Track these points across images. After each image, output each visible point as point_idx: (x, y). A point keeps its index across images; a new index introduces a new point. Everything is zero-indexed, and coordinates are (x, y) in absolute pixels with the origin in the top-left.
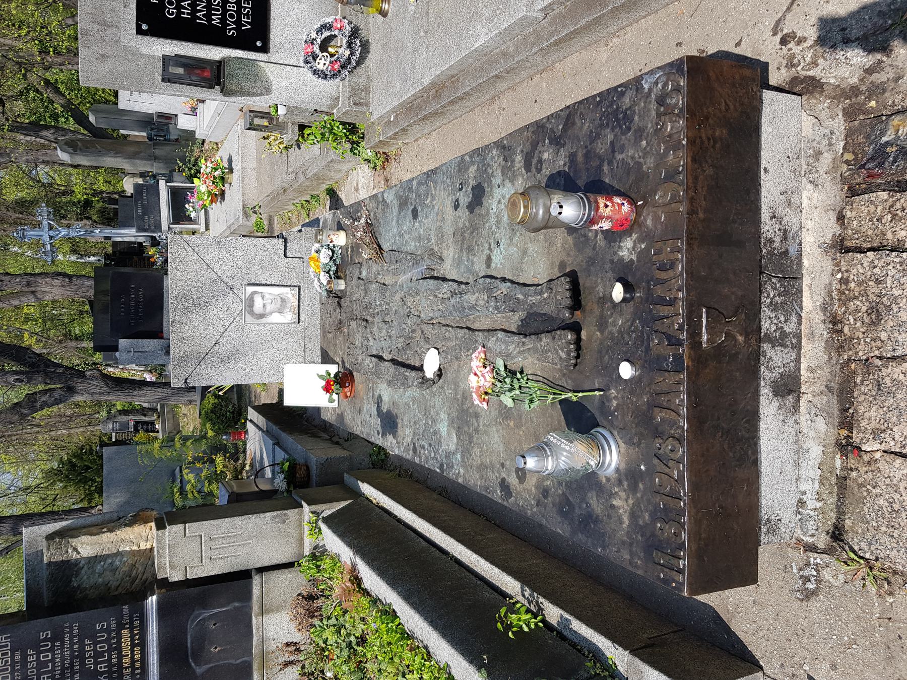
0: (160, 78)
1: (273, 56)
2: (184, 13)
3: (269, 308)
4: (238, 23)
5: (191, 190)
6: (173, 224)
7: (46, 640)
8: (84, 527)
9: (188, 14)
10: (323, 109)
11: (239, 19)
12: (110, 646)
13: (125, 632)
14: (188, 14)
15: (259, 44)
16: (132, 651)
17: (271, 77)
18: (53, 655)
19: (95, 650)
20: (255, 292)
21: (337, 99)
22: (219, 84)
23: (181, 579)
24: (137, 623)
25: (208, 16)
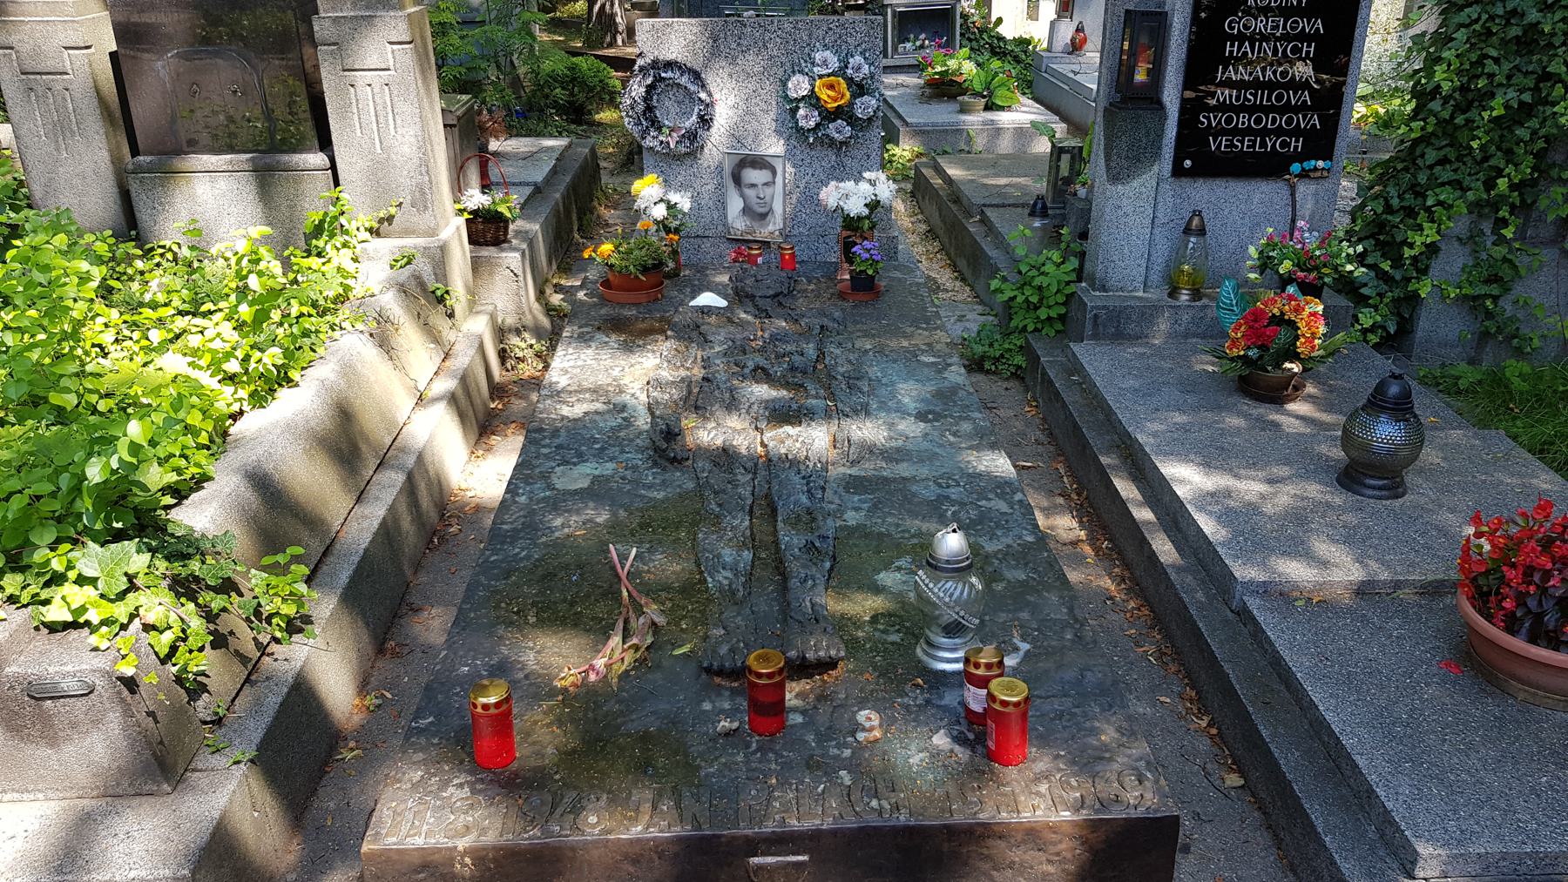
2: (1232, 46)
3: (750, 192)
6: (894, 13)
9: (1231, 52)
10: (1088, 265)
11: (1224, 132)
14: (1231, 52)
17: (1135, 184)
20: (774, 173)
21: (1104, 288)
22: (1123, 100)
23: (316, 36)
25: (1228, 83)
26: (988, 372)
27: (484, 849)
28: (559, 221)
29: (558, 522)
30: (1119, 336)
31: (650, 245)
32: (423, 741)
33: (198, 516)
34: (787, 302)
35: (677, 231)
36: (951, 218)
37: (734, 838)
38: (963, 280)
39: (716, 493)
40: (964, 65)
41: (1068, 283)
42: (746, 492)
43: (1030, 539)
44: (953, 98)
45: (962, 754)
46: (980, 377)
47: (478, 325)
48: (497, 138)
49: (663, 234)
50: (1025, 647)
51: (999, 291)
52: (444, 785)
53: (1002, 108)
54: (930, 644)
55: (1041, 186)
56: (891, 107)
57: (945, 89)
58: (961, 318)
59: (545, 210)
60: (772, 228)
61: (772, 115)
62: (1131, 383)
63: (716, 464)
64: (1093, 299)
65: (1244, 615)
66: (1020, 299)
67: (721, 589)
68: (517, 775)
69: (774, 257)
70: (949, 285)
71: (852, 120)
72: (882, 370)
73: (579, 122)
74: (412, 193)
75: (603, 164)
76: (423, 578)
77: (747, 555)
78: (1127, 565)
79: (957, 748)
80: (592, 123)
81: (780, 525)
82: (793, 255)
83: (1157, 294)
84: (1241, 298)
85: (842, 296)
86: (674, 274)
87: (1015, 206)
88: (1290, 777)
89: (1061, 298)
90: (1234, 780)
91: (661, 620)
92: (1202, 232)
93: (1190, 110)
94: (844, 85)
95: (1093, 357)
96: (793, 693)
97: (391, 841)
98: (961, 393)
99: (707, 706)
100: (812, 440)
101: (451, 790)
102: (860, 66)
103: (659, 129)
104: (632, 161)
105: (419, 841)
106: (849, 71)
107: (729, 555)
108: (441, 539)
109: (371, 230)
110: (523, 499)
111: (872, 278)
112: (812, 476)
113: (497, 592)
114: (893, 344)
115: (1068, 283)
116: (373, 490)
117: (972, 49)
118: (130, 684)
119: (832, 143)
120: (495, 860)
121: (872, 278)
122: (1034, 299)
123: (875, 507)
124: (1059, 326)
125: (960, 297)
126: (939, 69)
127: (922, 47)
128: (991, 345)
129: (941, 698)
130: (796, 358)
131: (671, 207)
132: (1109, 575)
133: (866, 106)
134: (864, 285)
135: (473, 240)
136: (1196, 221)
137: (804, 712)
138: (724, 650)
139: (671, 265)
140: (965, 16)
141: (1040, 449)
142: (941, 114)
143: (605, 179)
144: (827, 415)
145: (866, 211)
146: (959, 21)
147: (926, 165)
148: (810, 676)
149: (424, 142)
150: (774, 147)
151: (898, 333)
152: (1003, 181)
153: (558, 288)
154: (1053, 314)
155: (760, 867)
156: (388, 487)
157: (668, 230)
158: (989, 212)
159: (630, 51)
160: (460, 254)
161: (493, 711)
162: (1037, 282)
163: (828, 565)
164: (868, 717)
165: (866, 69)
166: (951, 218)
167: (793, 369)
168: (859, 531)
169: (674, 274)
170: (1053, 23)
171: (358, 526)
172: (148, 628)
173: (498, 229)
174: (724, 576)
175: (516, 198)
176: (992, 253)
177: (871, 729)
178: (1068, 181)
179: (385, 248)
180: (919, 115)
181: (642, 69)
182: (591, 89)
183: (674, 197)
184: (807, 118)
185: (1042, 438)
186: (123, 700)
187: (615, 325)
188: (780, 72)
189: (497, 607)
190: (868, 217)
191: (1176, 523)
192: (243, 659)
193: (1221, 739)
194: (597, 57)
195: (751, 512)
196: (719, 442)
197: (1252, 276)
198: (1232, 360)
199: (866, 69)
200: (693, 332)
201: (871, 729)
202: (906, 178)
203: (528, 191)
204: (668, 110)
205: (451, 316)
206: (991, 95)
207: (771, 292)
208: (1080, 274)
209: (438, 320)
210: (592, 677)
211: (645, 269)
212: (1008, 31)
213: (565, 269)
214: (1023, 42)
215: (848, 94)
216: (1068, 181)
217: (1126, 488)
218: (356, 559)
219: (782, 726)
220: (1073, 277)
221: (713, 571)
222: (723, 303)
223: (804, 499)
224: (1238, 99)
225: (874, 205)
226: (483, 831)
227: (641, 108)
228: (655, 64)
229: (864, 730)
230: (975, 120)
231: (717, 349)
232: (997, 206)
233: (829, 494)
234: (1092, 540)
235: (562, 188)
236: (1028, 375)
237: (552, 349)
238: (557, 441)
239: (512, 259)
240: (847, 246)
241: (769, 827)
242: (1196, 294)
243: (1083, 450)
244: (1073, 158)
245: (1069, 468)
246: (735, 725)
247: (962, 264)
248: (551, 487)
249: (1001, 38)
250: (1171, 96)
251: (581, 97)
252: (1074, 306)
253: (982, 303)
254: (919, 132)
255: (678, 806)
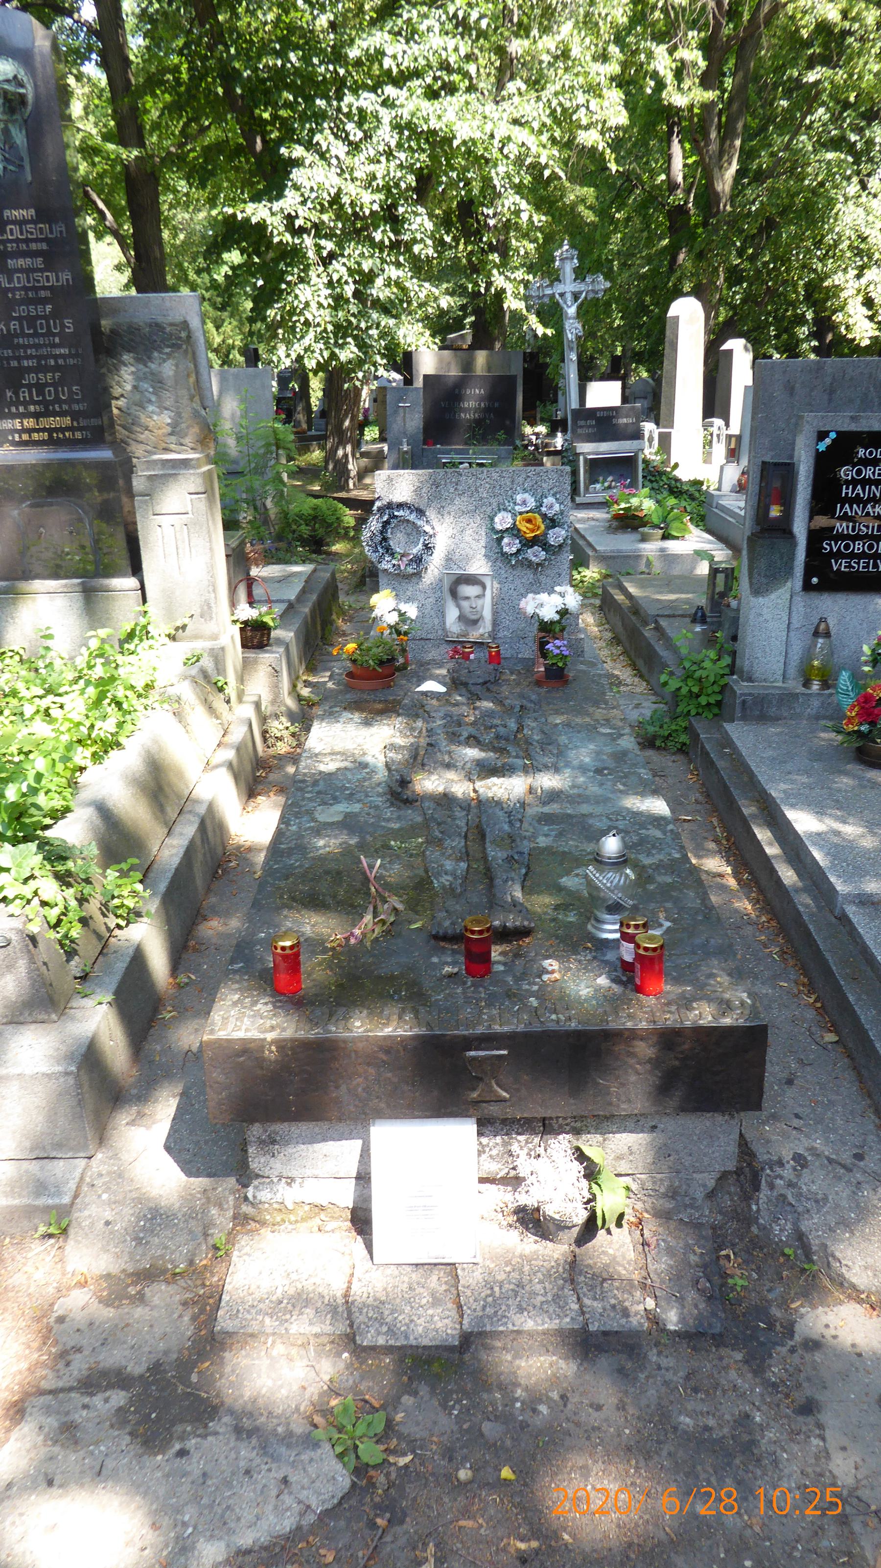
0: (768, 459)
1: (800, 601)
3: (465, 604)
4: (839, 555)
5: (633, 485)
6: (586, 460)
7: (63, 326)
8: (196, 366)
10: (738, 662)
12: (52, 403)
13: (67, 421)
15: (815, 580)
16: (44, 430)
18: (43, 335)
19: (47, 384)
20: (484, 587)
21: (750, 679)
22: (763, 531)
24: (78, 435)
26: (659, 748)
27: (284, 1040)
28: (307, 631)
29: (321, 843)
30: (763, 718)
31: (385, 644)
32: (237, 977)
33: (74, 831)
34: (494, 688)
35: (406, 634)
36: (631, 629)
37: (455, 1036)
38: (641, 676)
39: (439, 824)
40: (644, 502)
41: (723, 676)
42: (462, 823)
43: (677, 856)
44: (635, 529)
45: (617, 989)
46: (650, 753)
47: (247, 711)
48: (257, 565)
49: (395, 636)
50: (667, 924)
51: (665, 684)
52: (254, 1003)
53: (677, 538)
54: (598, 921)
55: (702, 601)
56: (583, 537)
57: (629, 522)
58: (637, 706)
59: (297, 623)
60: (484, 629)
61: (483, 543)
62: (770, 753)
63: (438, 804)
64: (742, 687)
65: (844, 919)
66: (684, 690)
67: (443, 887)
68: (303, 997)
69: (483, 655)
70: (629, 681)
71: (546, 546)
72: (569, 738)
73: (318, 552)
74: (202, 607)
75: (340, 586)
76: (213, 900)
77: (463, 865)
78: (761, 891)
79: (614, 986)
80: (329, 554)
81: (488, 844)
82: (498, 653)
83: (795, 685)
84: (855, 685)
85: (538, 683)
86: (404, 667)
87: (682, 616)
88: (867, 1027)
89: (716, 688)
90: (831, 1037)
91: (400, 907)
92: (827, 634)
93: (815, 537)
94: (539, 520)
95: (739, 733)
96: (496, 953)
97: (222, 1034)
98: (630, 756)
99: (435, 960)
100: (509, 788)
101: (259, 1006)
102: (552, 505)
103: (392, 555)
104: (368, 580)
105: (240, 1035)
106: (544, 509)
107: (449, 868)
108: (224, 871)
109: (169, 636)
110: (294, 828)
111: (562, 669)
112: (515, 812)
113: (279, 888)
114: (578, 720)
115: (723, 676)
116: (177, 829)
117: (652, 489)
118: (33, 939)
119: (530, 565)
120: (292, 1049)
121: (562, 669)
122: (695, 690)
123: (560, 834)
124: (716, 711)
125: (638, 690)
126: (623, 505)
127: (610, 487)
128: (661, 727)
129: (604, 955)
130: (501, 730)
131: (401, 615)
132: (748, 898)
133: (556, 536)
134: (557, 675)
135: (244, 646)
136: (822, 626)
137: (505, 964)
138: (447, 923)
139: (401, 660)
140: (646, 462)
141: (699, 807)
142: (624, 542)
143: (342, 598)
144: (526, 770)
145: (557, 617)
146: (641, 466)
147: (611, 585)
148: (510, 942)
149: (211, 567)
150: (479, 566)
151: (580, 711)
152: (672, 597)
153: (307, 684)
154: (712, 701)
155: (474, 1059)
156: (188, 830)
157: (399, 633)
158: (663, 623)
159: (363, 495)
160: (234, 652)
161: (288, 952)
162: (697, 675)
163: (524, 871)
164: (551, 964)
165: (557, 507)
166: (631, 629)
167: (498, 737)
168: (548, 851)
169: (404, 667)
170: (722, 468)
171: (169, 850)
172: (44, 904)
173: (262, 636)
174: (446, 880)
175: (278, 609)
176: (663, 653)
177: (553, 972)
178: (723, 595)
179: (183, 649)
180: (608, 543)
181: (379, 509)
182: (330, 525)
183: (403, 607)
184: (510, 546)
185: (701, 798)
186: (29, 951)
187: (356, 706)
188: (489, 510)
189: (281, 897)
190: (559, 622)
191: (798, 856)
192: (99, 937)
193: (822, 1011)
194: (335, 498)
195: (466, 837)
196: (441, 789)
197: (867, 669)
198: (849, 734)
199: (557, 507)
200: (417, 709)
201: (553, 972)
202: (595, 595)
203: (284, 606)
204: (398, 541)
205: (228, 702)
206: (667, 527)
207: (481, 681)
208: (732, 669)
209: (218, 702)
210: (353, 941)
211: (381, 663)
212: (684, 474)
213: (312, 669)
214: (697, 483)
215: (543, 527)
216: (723, 595)
217: (763, 835)
218: (170, 875)
219: (488, 971)
220: (727, 671)
221: (438, 875)
222: (442, 689)
223: (506, 827)
224: (853, 530)
225: (564, 613)
226: (284, 1030)
227: (379, 538)
228: (390, 506)
229: (548, 972)
230: (651, 548)
231: (439, 722)
232: (669, 616)
233: (525, 825)
234: (736, 874)
235: (310, 604)
236: (688, 749)
237: (308, 729)
238: (317, 789)
239: (268, 658)
240: (542, 645)
241: (480, 1030)
242: (825, 685)
243: (730, 806)
244: (727, 577)
245: (721, 820)
246: (456, 970)
247: (640, 663)
248: (314, 820)
249: (677, 480)
250: (800, 528)
251: (321, 532)
252: (727, 694)
253: (656, 694)
254: (603, 559)
255: (416, 1017)
